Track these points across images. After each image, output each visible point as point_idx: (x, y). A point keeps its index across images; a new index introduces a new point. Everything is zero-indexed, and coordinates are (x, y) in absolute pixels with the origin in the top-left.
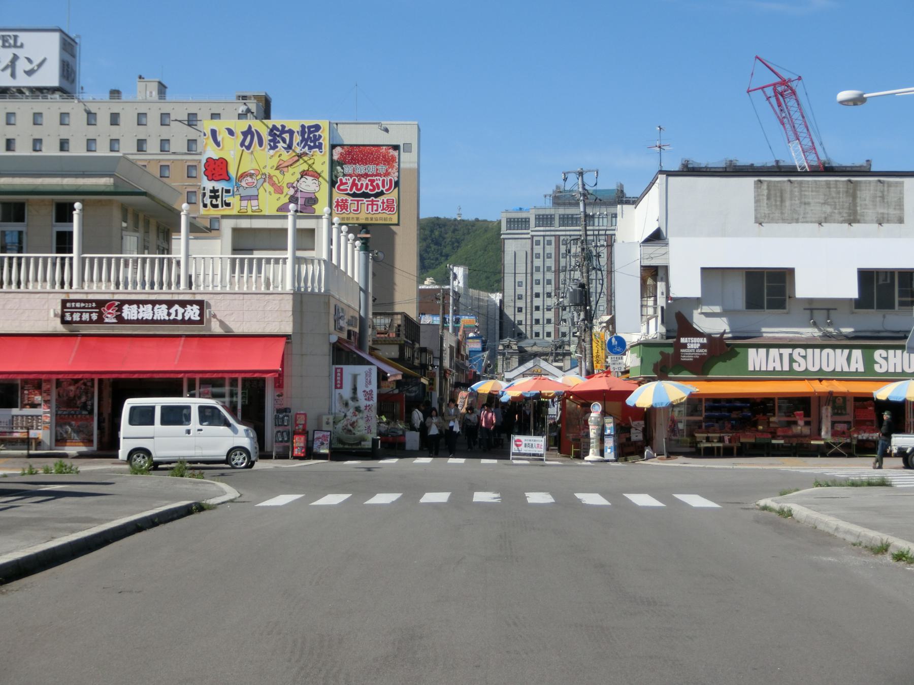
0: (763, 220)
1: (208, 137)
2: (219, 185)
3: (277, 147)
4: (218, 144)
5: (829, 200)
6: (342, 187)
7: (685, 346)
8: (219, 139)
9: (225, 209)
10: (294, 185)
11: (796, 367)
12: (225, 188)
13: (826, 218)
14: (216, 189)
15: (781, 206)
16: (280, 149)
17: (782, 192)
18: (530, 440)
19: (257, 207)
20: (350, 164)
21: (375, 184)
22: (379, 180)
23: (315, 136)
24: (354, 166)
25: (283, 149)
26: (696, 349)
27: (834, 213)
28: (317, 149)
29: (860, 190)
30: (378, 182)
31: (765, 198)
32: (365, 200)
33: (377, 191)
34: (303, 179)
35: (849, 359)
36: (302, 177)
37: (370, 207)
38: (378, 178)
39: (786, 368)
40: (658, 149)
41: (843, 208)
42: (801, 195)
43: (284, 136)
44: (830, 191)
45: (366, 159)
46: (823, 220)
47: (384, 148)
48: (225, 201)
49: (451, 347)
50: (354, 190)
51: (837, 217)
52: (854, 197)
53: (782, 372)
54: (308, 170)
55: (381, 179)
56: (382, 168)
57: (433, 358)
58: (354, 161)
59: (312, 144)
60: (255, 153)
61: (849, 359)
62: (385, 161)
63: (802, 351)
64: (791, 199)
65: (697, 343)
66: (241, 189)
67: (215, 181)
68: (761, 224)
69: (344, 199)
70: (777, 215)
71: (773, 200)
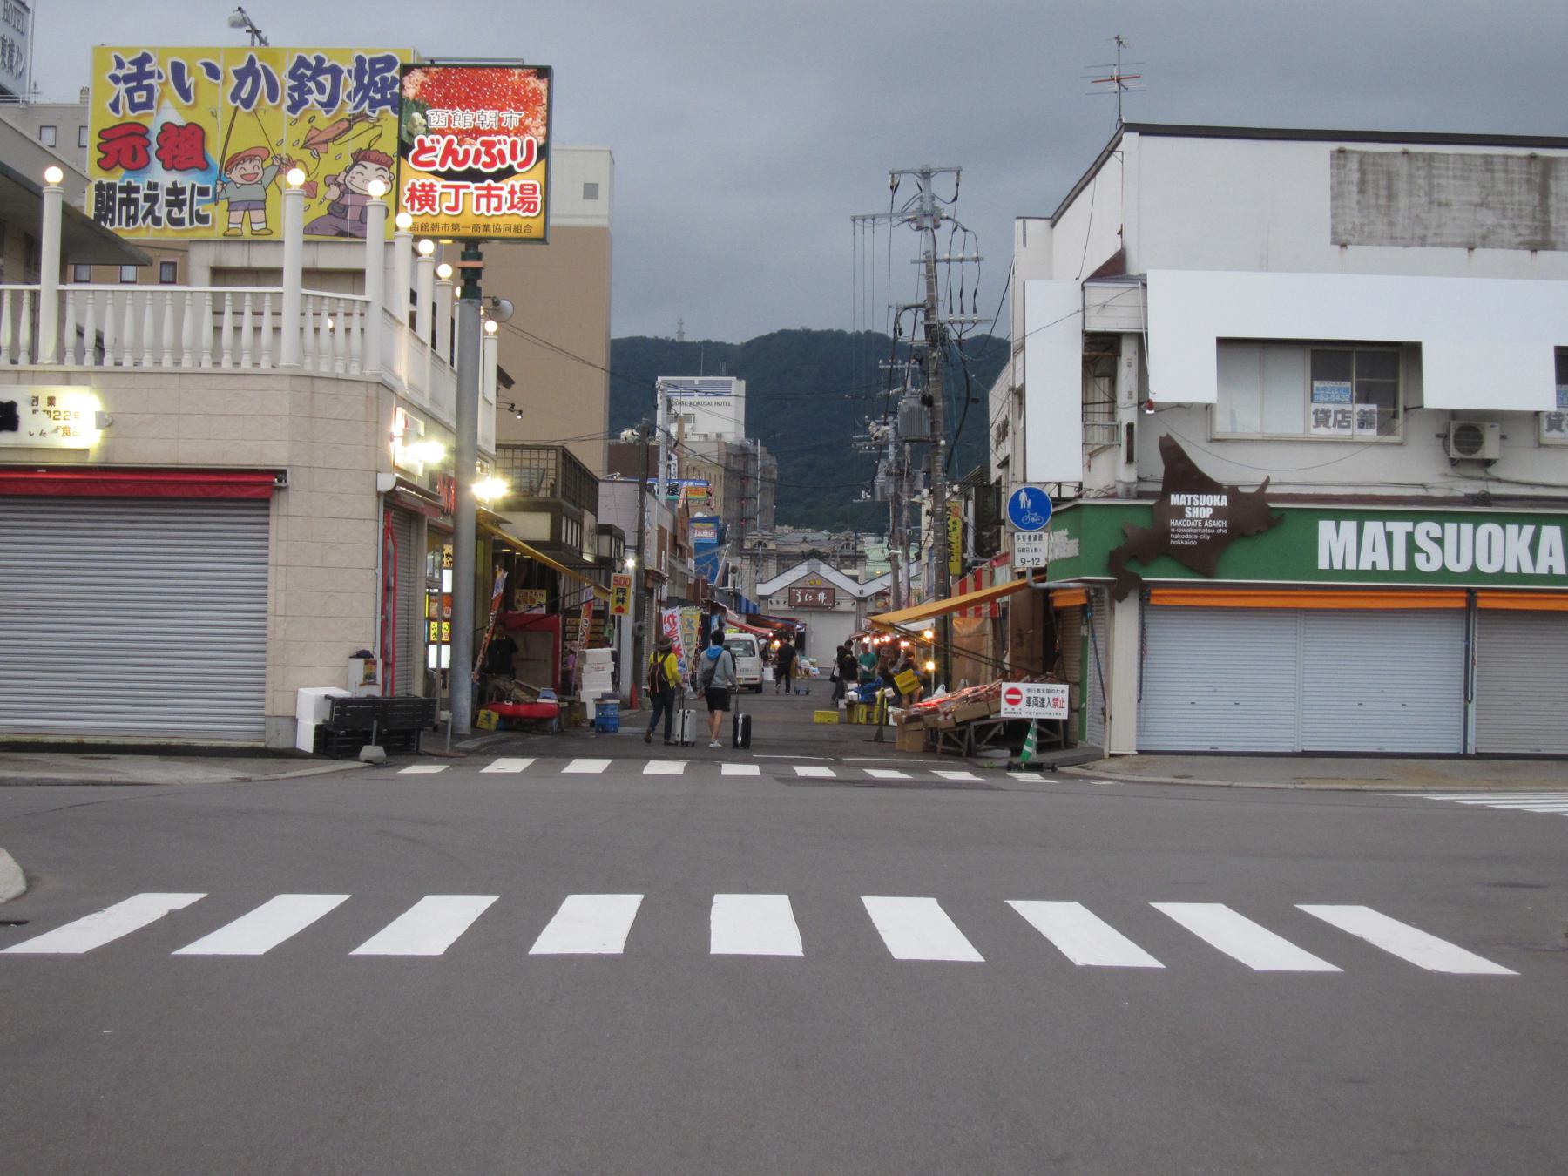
0: (1349, 238)
1: (167, 81)
2: (186, 180)
3: (306, 102)
4: (185, 94)
5: (1490, 199)
6: (422, 158)
7: (1179, 512)
8: (189, 82)
9: (197, 228)
10: (340, 180)
11: (1420, 561)
12: (197, 185)
13: (1484, 238)
14: (179, 186)
15: (1389, 207)
16: (313, 105)
17: (1390, 177)
18: (1038, 691)
19: (263, 226)
20: (441, 106)
21: (494, 151)
22: (505, 142)
23: (384, 80)
24: (450, 112)
25: (319, 107)
26: (1204, 520)
27: (1502, 226)
28: (389, 107)
29: (1557, 179)
30: (502, 147)
31: (1354, 189)
32: (473, 185)
33: (499, 166)
34: (358, 168)
35: (1534, 547)
36: (356, 163)
37: (483, 201)
38: (502, 138)
39: (1400, 564)
40: (1115, 86)
41: (1521, 217)
42: (1431, 186)
43: (321, 78)
44: (1493, 179)
45: (475, 97)
46: (1478, 241)
47: (517, 71)
48: (198, 211)
49: (661, 530)
50: (449, 163)
51: (1508, 235)
52: (1544, 192)
53: (1391, 574)
54: (369, 149)
55: (509, 141)
56: (512, 118)
57: (625, 547)
58: (448, 102)
59: (378, 97)
60: (260, 114)
61: (1534, 547)
62: (520, 101)
63: (1434, 528)
64: (1410, 194)
65: (1206, 506)
66: (230, 188)
67: (177, 170)
68: (1343, 245)
69: (428, 183)
70: (1380, 227)
71: (1371, 192)
